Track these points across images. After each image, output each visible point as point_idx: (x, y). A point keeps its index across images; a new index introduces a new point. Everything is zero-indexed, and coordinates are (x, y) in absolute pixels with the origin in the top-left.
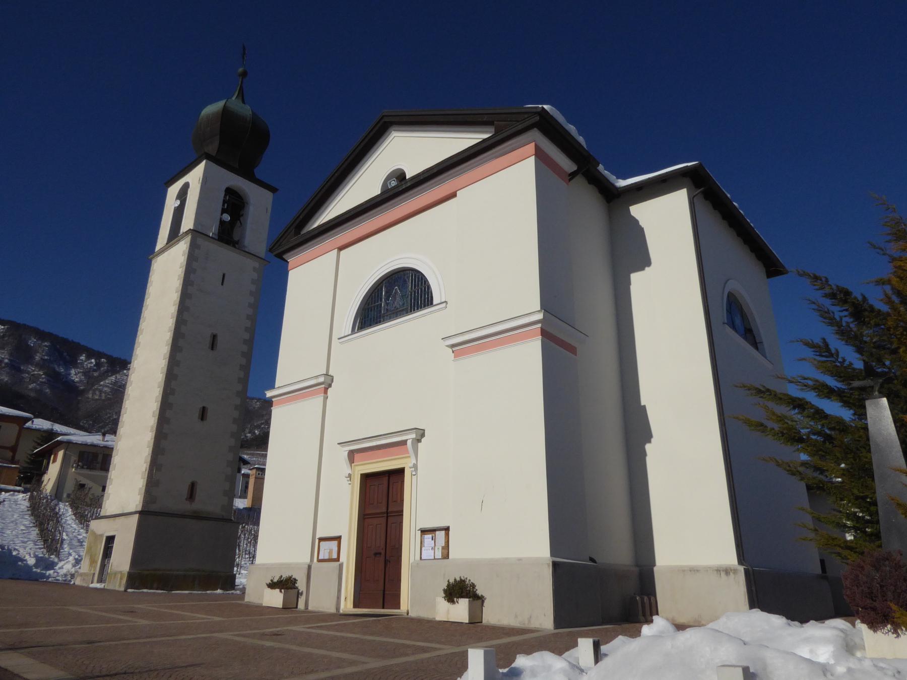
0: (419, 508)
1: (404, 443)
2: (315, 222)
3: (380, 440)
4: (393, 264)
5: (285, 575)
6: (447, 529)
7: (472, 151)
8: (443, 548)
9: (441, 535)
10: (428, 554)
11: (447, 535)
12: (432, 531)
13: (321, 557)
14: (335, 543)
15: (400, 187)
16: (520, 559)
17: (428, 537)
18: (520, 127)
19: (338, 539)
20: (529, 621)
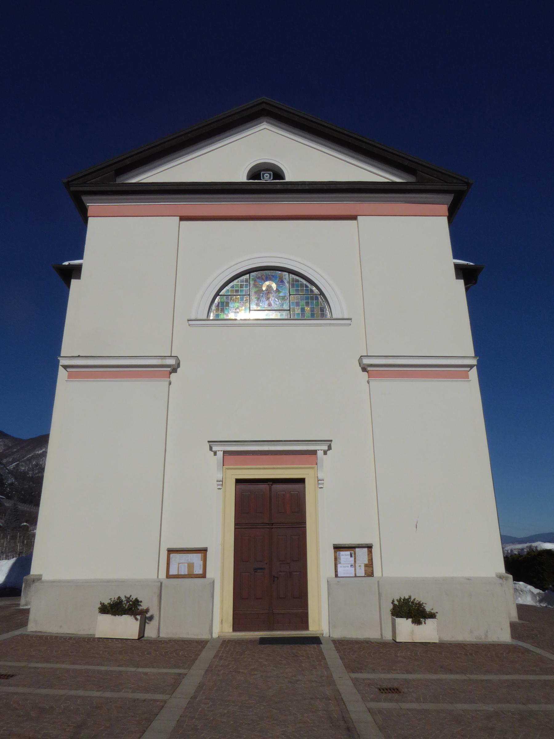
0: (325, 525)
1: (314, 452)
2: (133, 177)
3: (285, 445)
4: (298, 265)
5: (123, 594)
6: (369, 547)
7: (362, 187)
8: (366, 566)
9: (362, 553)
10: (345, 570)
11: (370, 553)
12: (351, 548)
13: (173, 571)
14: (199, 556)
15: (266, 186)
16: (469, 579)
17: (345, 555)
18: (446, 187)
19: (203, 551)
20: (486, 636)
